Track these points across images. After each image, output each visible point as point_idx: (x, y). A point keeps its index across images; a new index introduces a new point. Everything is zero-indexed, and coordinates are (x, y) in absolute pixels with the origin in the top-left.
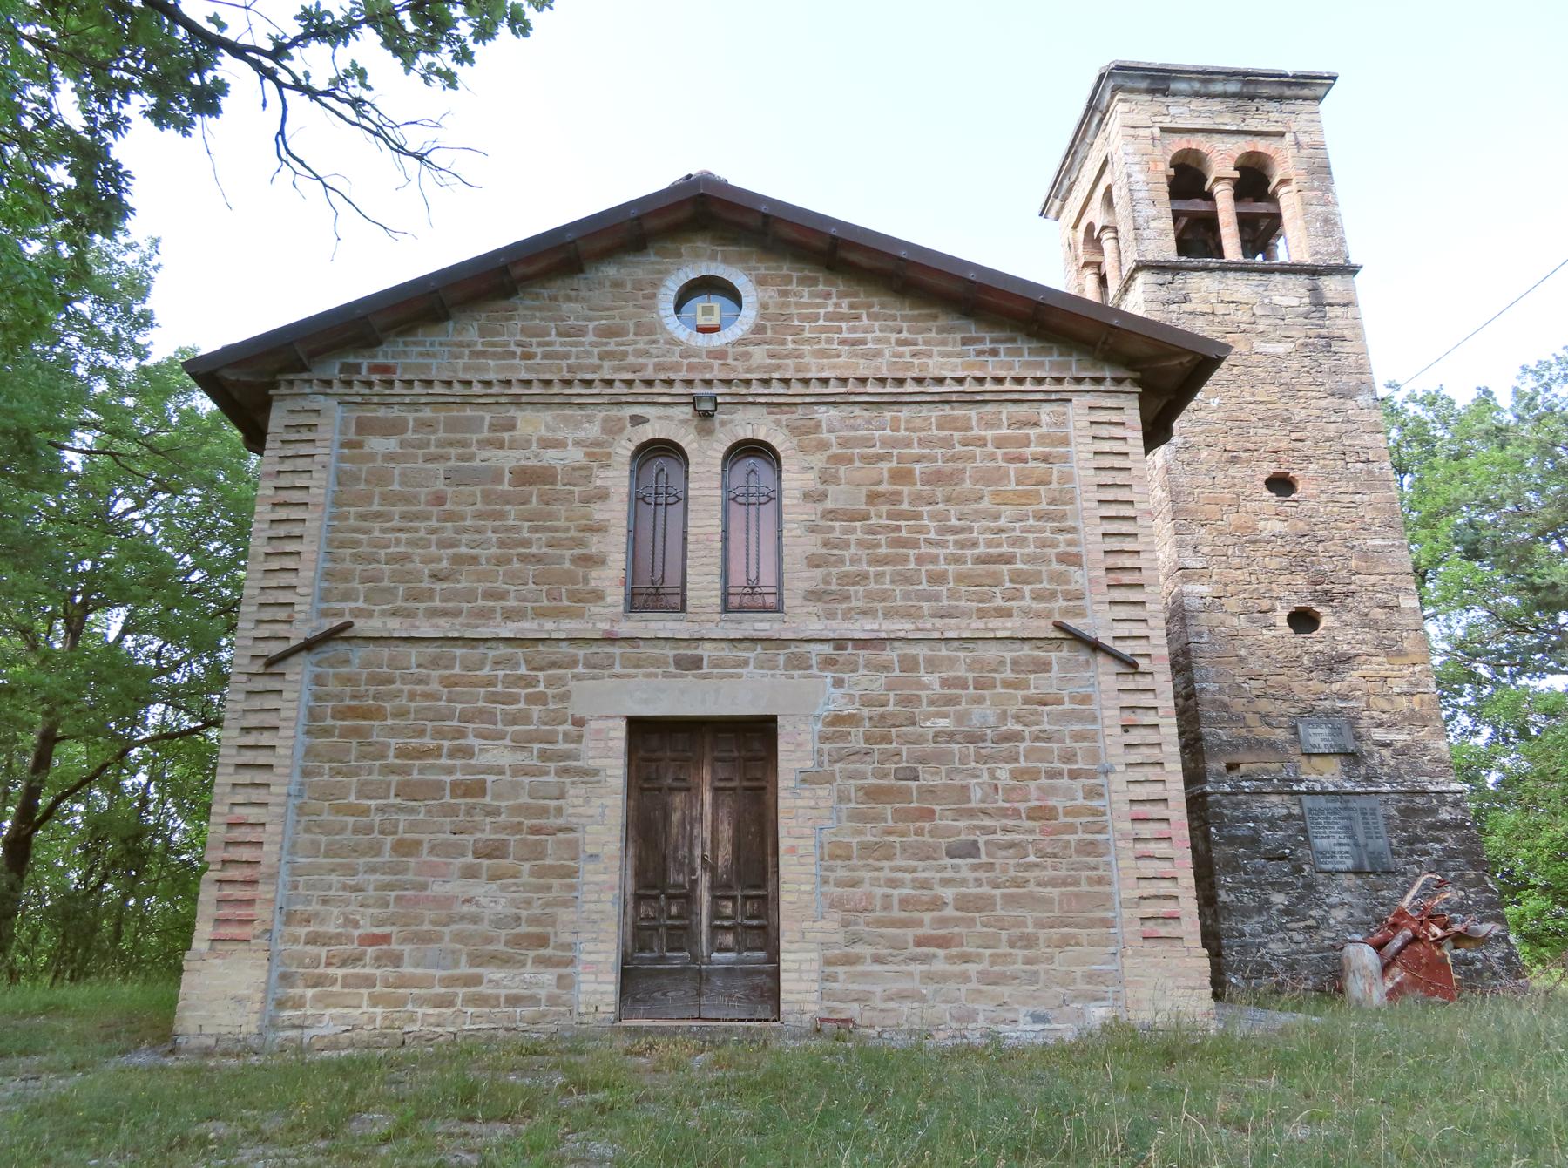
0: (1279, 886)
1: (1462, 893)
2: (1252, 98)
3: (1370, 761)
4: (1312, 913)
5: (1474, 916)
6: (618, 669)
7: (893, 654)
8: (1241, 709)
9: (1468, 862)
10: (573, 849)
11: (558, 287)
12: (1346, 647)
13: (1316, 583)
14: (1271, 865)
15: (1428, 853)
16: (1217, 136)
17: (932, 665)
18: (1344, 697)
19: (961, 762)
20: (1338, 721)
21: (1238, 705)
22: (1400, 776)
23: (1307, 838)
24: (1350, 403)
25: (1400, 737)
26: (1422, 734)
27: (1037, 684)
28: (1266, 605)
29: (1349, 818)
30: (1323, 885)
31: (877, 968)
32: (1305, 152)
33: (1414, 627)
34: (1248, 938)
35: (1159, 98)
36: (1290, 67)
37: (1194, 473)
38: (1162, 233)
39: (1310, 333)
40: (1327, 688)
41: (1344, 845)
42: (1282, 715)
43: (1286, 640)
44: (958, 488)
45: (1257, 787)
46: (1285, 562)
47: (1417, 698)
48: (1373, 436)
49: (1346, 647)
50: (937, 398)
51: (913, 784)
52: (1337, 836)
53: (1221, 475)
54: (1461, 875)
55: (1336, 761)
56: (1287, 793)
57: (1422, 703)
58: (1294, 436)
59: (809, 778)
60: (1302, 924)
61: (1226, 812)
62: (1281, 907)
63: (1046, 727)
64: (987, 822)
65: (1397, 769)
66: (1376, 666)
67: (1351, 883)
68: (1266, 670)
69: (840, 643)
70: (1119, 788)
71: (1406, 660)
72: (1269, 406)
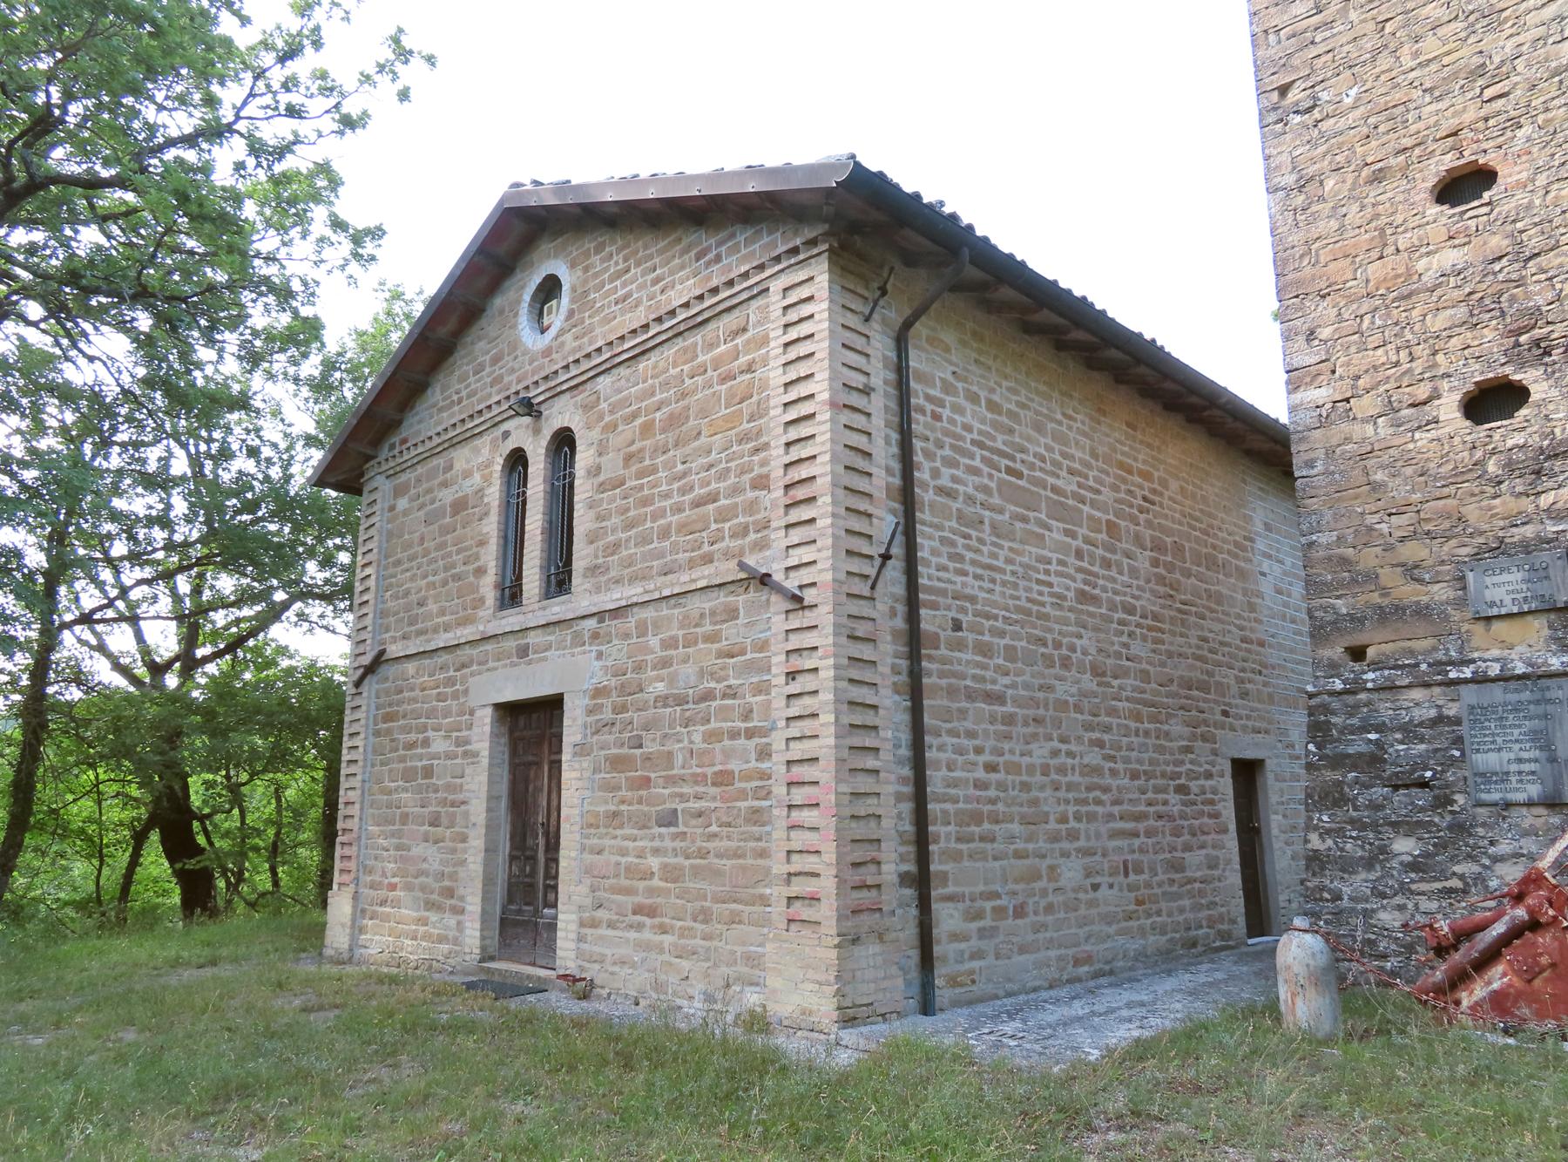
4: (1457, 869)
6: (491, 664)
8: (1373, 562)
11: (474, 332)
14: (1400, 797)
19: (670, 727)
20: (1544, 557)
21: (1369, 558)
23: (1463, 754)
28: (1422, 392)
30: (1484, 825)
31: (610, 932)
34: (1345, 903)
37: (1315, 218)
40: (1527, 505)
41: (1529, 761)
42: (1443, 562)
43: (1457, 440)
44: (684, 428)
45: (1387, 679)
46: (1461, 312)
50: (670, 334)
51: (638, 752)
52: (1516, 747)
53: (1355, 207)
56: (1440, 684)
58: (1488, 93)
60: (1438, 885)
61: (1334, 720)
63: (732, 682)
64: (686, 790)
67: (1539, 822)
68: (1417, 496)
72: (1446, 60)
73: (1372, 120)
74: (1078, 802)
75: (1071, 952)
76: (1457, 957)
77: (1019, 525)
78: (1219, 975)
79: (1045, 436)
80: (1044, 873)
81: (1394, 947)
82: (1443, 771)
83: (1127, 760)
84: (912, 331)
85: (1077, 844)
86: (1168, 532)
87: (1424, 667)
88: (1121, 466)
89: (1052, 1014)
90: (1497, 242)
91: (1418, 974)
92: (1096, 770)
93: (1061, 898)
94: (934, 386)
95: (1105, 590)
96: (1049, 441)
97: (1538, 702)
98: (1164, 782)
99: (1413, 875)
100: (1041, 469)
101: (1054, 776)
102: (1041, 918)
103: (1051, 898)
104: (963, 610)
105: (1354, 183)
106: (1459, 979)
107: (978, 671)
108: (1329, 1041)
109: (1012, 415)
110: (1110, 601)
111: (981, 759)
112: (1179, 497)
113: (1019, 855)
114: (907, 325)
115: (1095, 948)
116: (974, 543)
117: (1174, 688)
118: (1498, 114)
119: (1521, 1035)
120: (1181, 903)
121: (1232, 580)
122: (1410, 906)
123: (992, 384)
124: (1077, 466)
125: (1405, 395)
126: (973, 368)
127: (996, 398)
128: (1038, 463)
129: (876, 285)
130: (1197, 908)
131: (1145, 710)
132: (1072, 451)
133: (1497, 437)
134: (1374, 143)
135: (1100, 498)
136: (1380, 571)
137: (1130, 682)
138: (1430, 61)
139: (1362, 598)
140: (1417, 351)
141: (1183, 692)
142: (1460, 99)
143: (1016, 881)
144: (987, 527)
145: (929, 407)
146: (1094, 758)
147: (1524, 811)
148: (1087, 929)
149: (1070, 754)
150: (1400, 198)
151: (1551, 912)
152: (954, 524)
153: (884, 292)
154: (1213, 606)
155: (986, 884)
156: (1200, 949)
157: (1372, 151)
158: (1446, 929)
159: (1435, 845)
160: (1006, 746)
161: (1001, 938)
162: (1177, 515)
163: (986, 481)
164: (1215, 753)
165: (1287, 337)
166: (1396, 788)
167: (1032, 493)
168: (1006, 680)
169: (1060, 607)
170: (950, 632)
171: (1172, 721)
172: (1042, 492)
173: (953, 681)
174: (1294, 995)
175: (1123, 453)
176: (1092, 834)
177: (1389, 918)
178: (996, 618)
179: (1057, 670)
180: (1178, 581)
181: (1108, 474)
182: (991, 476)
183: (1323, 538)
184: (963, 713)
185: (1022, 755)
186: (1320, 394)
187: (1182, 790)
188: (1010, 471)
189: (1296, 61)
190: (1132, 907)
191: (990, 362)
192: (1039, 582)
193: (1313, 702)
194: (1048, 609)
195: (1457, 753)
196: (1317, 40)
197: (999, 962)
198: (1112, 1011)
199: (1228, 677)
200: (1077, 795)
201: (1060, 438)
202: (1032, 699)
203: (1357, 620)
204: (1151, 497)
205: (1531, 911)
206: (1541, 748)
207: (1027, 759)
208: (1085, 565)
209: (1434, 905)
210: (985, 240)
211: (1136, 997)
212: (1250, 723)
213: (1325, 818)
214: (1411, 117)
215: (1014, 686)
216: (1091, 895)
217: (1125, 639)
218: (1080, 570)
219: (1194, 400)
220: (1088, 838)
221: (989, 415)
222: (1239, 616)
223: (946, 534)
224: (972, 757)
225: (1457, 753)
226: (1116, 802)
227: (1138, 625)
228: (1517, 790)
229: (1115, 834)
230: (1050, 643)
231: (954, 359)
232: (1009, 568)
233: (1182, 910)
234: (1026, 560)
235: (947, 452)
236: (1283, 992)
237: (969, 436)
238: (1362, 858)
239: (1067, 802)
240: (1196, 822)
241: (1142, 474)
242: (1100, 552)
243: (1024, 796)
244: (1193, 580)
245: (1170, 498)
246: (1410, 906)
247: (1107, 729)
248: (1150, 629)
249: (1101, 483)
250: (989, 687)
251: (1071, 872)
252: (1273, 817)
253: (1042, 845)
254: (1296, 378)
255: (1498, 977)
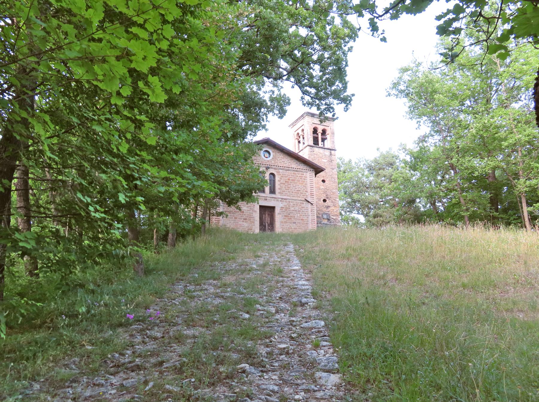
7: (288, 201)
10: (254, 220)
17: (292, 202)
25: (334, 218)
27: (302, 205)
59: (279, 214)
66: (333, 208)
69: (282, 199)
70: (310, 218)
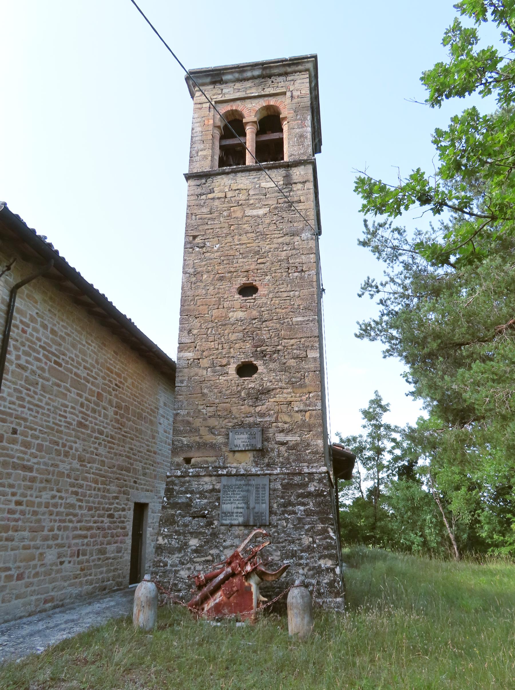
0: (195, 534)
1: (311, 539)
2: (270, 77)
3: (272, 454)
4: (211, 552)
5: (317, 555)
8: (198, 424)
9: (319, 519)
12: (268, 384)
13: (257, 347)
15: (294, 513)
16: (248, 101)
18: (262, 415)
20: (255, 430)
21: (197, 423)
22: (289, 463)
24: (297, 238)
26: (307, 436)
28: (224, 361)
29: (248, 491)
30: (223, 533)
32: (295, 101)
33: (313, 369)
34: (168, 567)
35: (218, 86)
36: (287, 55)
37: (198, 288)
38: (205, 157)
39: (280, 201)
41: (241, 508)
43: (233, 382)
46: (241, 335)
47: (308, 414)
48: (308, 256)
49: (268, 384)
52: (237, 502)
53: (212, 288)
54: (312, 528)
55: (250, 455)
56: (215, 476)
57: (311, 416)
58: (259, 261)
60: (203, 559)
61: (176, 488)
62: (194, 548)
65: (288, 459)
71: (305, 390)
72: (248, 245)
73: (222, 258)
74: (60, 521)
75: (43, 597)
76: (205, 589)
77: (55, 388)
78: (112, 603)
79: (76, 350)
80: (37, 557)
81: (184, 586)
82: (212, 511)
83: (88, 502)
84: (20, 290)
85: (56, 542)
86: (124, 401)
87: (210, 468)
88: (108, 369)
89: (27, 629)
90: (255, 313)
91: (192, 597)
92: (72, 506)
93: (43, 569)
94: (26, 317)
95: (91, 422)
96: (78, 353)
97: (246, 485)
98: (103, 512)
99: (195, 555)
100: (71, 364)
101: (51, 508)
102: (31, 580)
103: (38, 569)
104: (19, 424)
105: (213, 279)
106: (205, 599)
107: (21, 455)
108: (150, 631)
109: (61, 337)
110: (92, 428)
111: (14, 499)
112: (131, 387)
113: (25, 548)
114: (18, 286)
115: (56, 594)
116: (31, 393)
117: (115, 469)
118: (261, 269)
119: (223, 621)
120: (101, 569)
121: (147, 425)
122: (192, 568)
123: (55, 322)
124: (88, 366)
125: (217, 361)
126: (47, 313)
127: (56, 329)
128: (70, 362)
129: (5, 264)
130: (108, 571)
131: (100, 479)
132: (88, 359)
133: (246, 383)
134: (222, 267)
135: (97, 381)
136: (200, 428)
137: (95, 465)
138: (243, 244)
139: (193, 438)
140: (225, 346)
141: (118, 471)
142: (250, 260)
143: (21, 561)
144: (39, 387)
145: (21, 326)
146: (72, 500)
147: (236, 528)
148: (54, 584)
149: (61, 498)
150: (227, 288)
151: (239, 569)
152: (23, 383)
153: (9, 268)
154: (137, 435)
155: (4, 563)
156: (107, 591)
157: (221, 269)
158: (203, 578)
159: (205, 542)
160: (29, 493)
161: (7, 591)
162: (129, 394)
163: (43, 365)
164: (128, 500)
165: (181, 330)
166: (194, 518)
167: (65, 374)
168: (35, 460)
169: (68, 428)
170: (10, 435)
171: (111, 485)
172: (70, 375)
173: (6, 459)
174: (139, 611)
175: (110, 364)
176: (65, 536)
177: (184, 574)
178: (35, 430)
179: (62, 457)
180: (125, 423)
181: (102, 372)
182: (46, 363)
183: (182, 412)
184: (9, 475)
185: (36, 497)
186: (189, 355)
187: (111, 516)
188: (56, 362)
189: (200, 228)
190: (78, 572)
191: (56, 312)
192: (60, 415)
193: (169, 480)
194: (62, 428)
195: (217, 504)
196: (209, 223)
197: (3, 605)
198: (57, 625)
199: (138, 466)
200: (61, 518)
201: (84, 353)
202: (46, 470)
203: (190, 447)
204: (119, 384)
205: (233, 569)
206: (245, 503)
207: (38, 500)
208: (84, 410)
209: (201, 567)
210: (63, 259)
211: (71, 617)
212: (145, 487)
213: (166, 530)
214: (235, 261)
215: (38, 463)
216: (59, 567)
217: (96, 445)
218: (81, 412)
219: (143, 347)
220: (62, 539)
221: (51, 336)
222: (147, 441)
223: (17, 387)
224: (9, 497)
225: (217, 504)
226: (79, 522)
227: (104, 440)
228: (235, 519)
229: (75, 537)
230: (60, 445)
231: (38, 307)
232: (47, 407)
233: (101, 573)
234: (56, 404)
235: (26, 348)
236: (135, 610)
237: (39, 343)
238: (177, 547)
239: (55, 521)
240: (115, 531)
241: (117, 374)
242: (92, 405)
243: (34, 518)
244: (131, 423)
245: (127, 386)
246: (192, 568)
247: (81, 486)
248: (109, 442)
249: (98, 375)
250: (25, 463)
251: (51, 556)
252: (149, 529)
253: (38, 542)
254: (182, 347)
255: (219, 597)
